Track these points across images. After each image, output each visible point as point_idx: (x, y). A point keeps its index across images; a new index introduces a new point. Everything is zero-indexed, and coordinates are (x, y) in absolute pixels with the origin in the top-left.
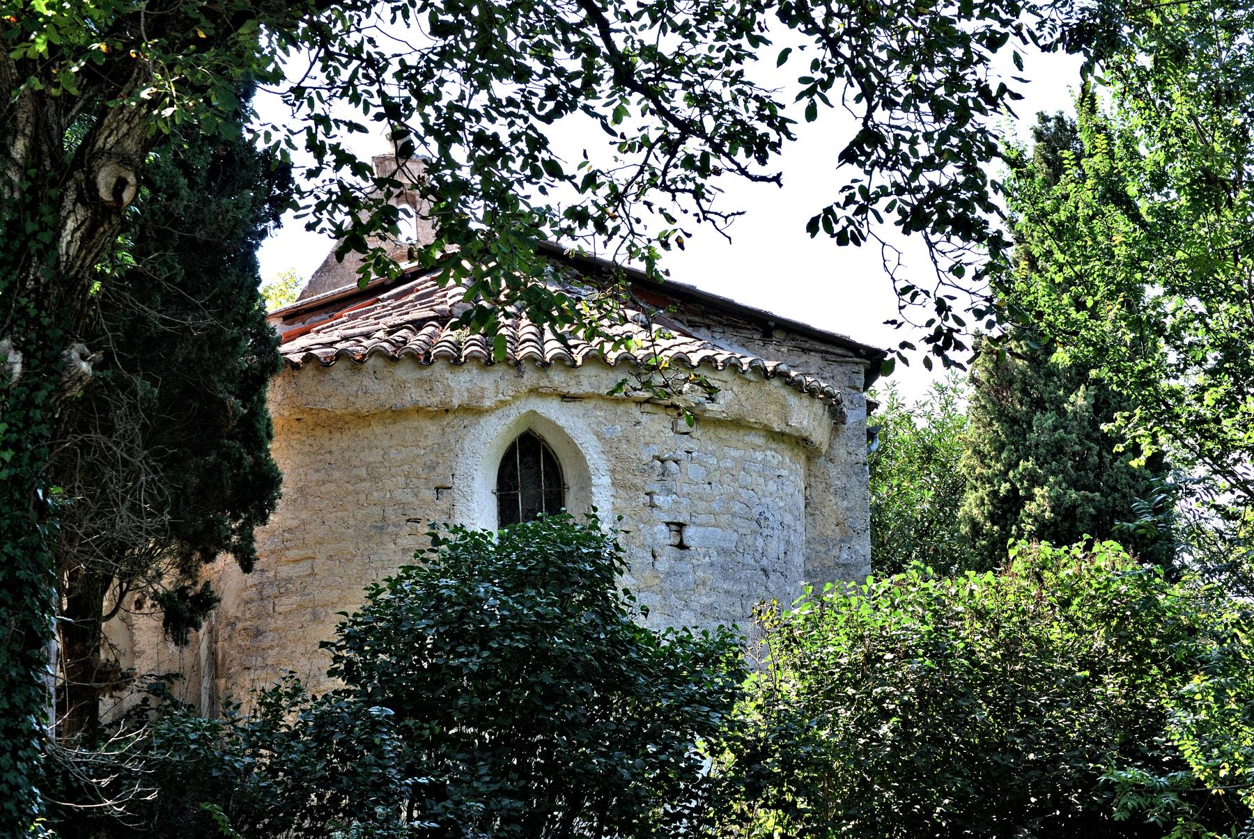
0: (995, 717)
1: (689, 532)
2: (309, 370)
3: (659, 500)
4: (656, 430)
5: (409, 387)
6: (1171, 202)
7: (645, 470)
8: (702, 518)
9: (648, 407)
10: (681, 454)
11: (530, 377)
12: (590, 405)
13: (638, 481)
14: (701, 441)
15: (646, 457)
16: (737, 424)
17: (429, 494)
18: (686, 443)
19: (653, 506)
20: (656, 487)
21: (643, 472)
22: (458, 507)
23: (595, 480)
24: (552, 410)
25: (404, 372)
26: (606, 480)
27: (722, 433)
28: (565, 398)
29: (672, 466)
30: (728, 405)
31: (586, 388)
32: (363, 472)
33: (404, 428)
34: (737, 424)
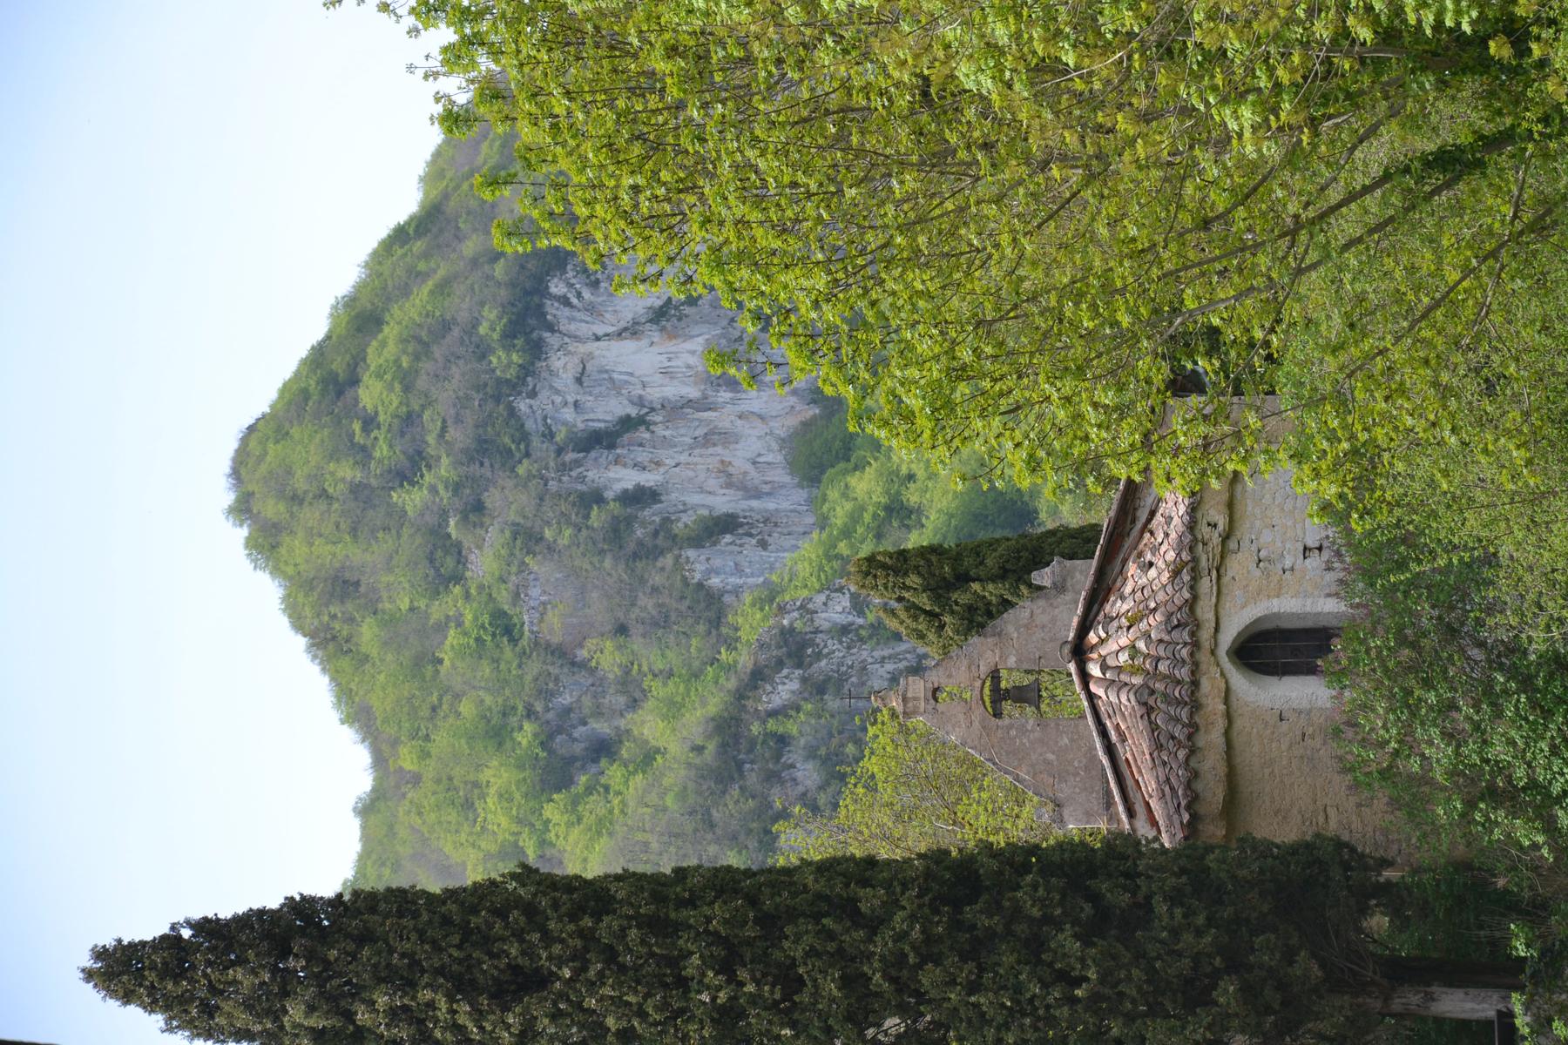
0: (1439, 570)
1: (1311, 543)
2: (1197, 807)
3: (1288, 563)
4: (1240, 565)
5: (1212, 738)
6: (847, 533)
7: (1267, 574)
8: (1299, 532)
9: (1222, 571)
10: (1254, 548)
11: (1204, 657)
12: (1222, 612)
13: (1275, 579)
14: (1244, 531)
15: (1258, 573)
16: (1231, 505)
17: (1285, 726)
18: (1245, 543)
19: (1292, 569)
20: (1279, 566)
21: (1268, 576)
22: (1295, 706)
23: (1275, 610)
24: (1228, 637)
25: (1201, 741)
26: (1275, 601)
27: (1237, 516)
28: (1217, 629)
29: (1263, 554)
30: (1219, 513)
31: (1211, 616)
32: (1267, 771)
33: (1238, 741)
34: (1231, 505)
